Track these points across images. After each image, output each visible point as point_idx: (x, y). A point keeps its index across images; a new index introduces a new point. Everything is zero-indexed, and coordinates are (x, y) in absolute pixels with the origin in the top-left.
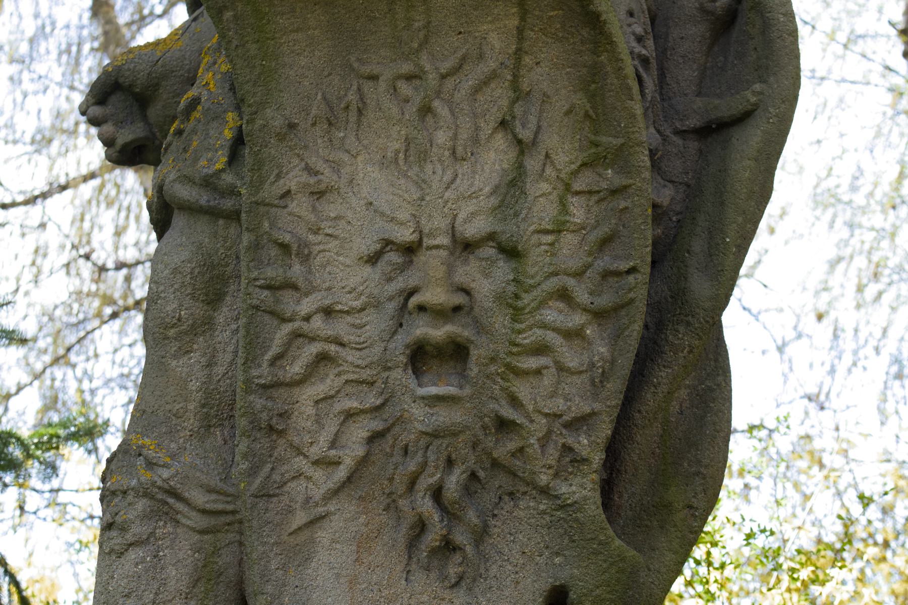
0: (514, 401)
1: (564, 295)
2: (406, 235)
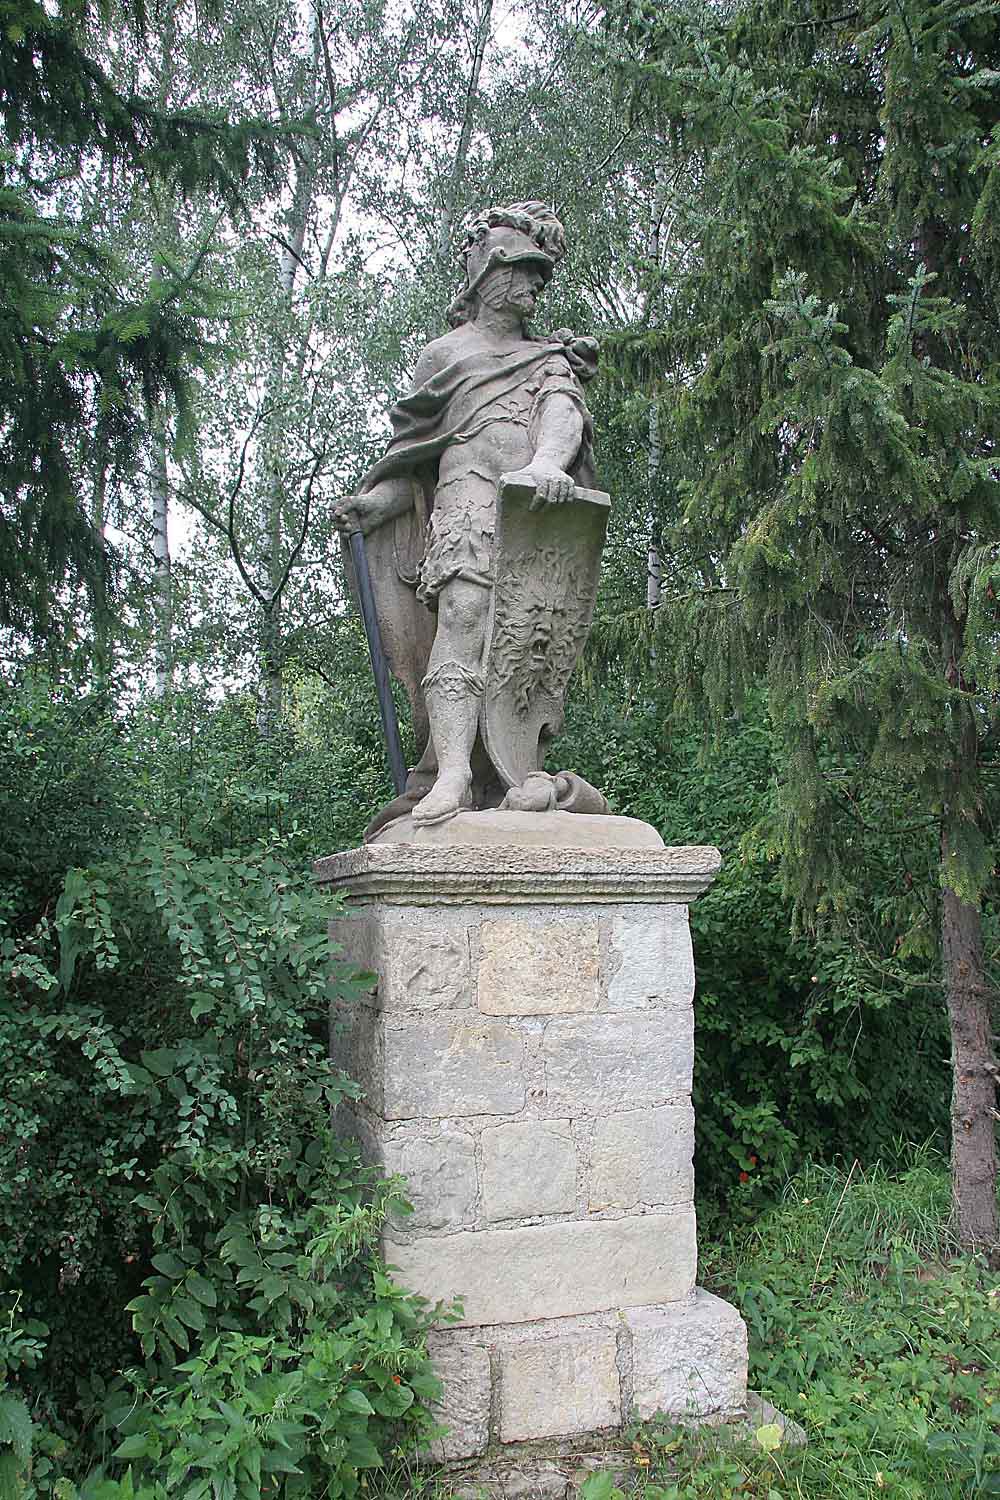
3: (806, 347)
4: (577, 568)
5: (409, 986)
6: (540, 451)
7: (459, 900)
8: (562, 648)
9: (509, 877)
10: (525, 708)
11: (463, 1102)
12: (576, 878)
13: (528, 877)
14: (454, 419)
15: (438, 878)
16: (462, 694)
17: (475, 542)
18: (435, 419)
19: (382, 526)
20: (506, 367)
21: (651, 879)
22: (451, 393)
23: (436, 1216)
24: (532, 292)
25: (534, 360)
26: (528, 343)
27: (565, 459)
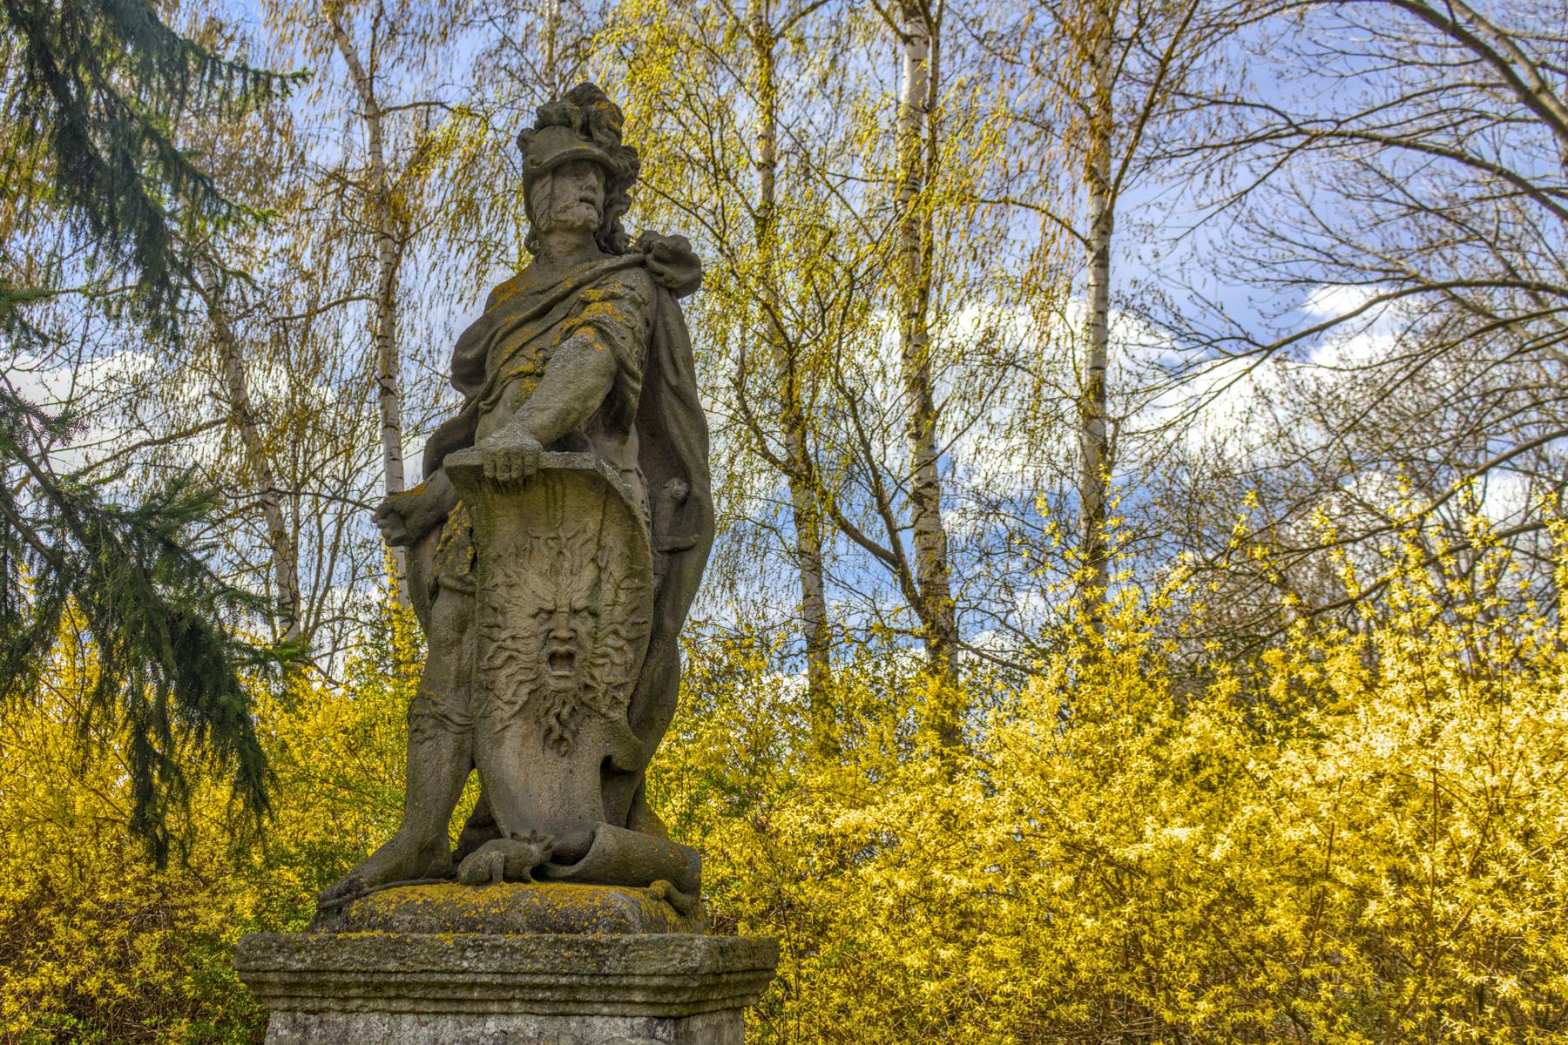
1: (616, 632)
2: (550, 606)
10: (562, 739)
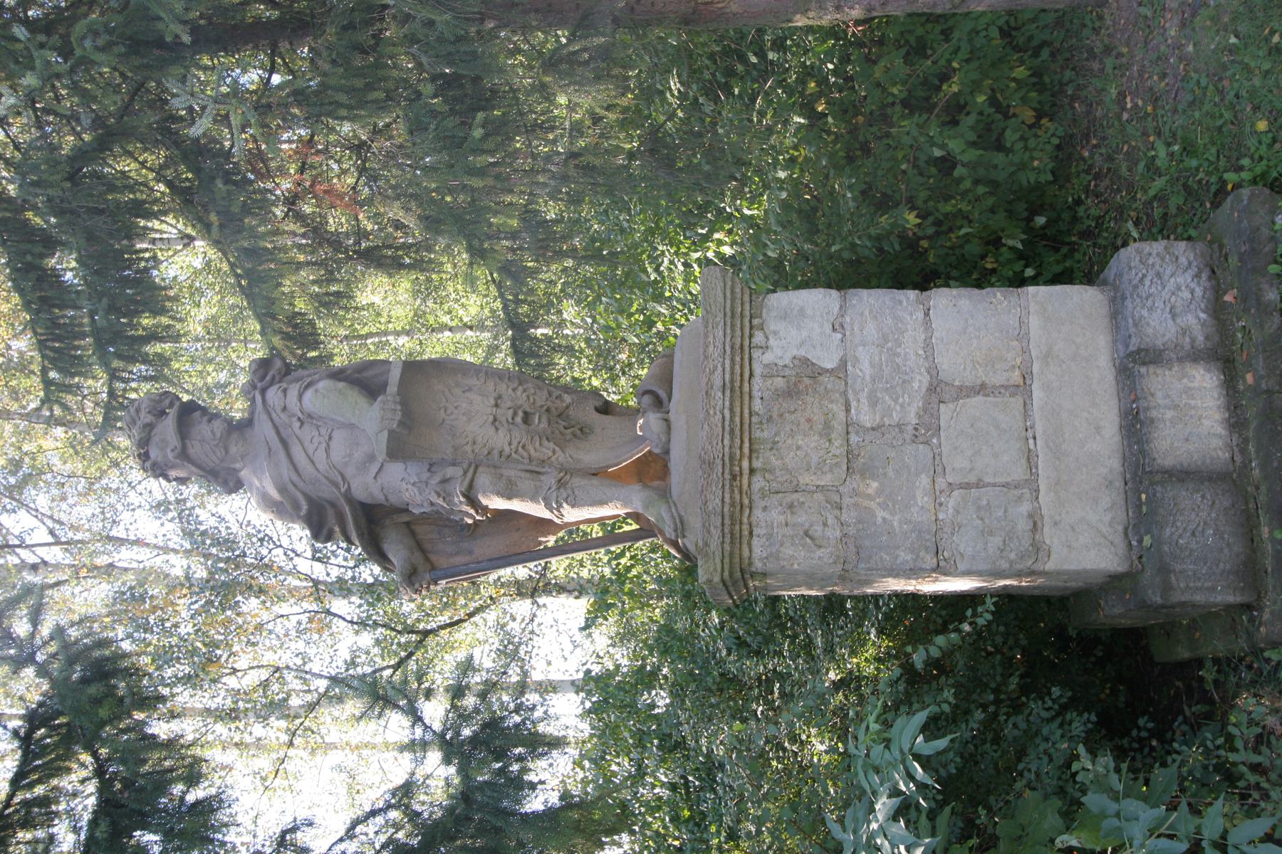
0: (542, 406)
1: (514, 390)
2: (491, 418)
3: (203, 108)
4: (457, 385)
5: (820, 547)
6: (353, 421)
7: (746, 502)
8: (528, 397)
9: (727, 459)
10: (581, 430)
11: (923, 499)
12: (727, 399)
13: (726, 442)
14: (327, 492)
15: (727, 521)
16: (569, 492)
17: (437, 479)
18: (328, 507)
19: (423, 551)
20: (279, 446)
21: (728, 331)
22: (305, 494)
23: (1023, 525)
24: (209, 421)
25: (272, 420)
26: (256, 421)
27: (362, 401)
